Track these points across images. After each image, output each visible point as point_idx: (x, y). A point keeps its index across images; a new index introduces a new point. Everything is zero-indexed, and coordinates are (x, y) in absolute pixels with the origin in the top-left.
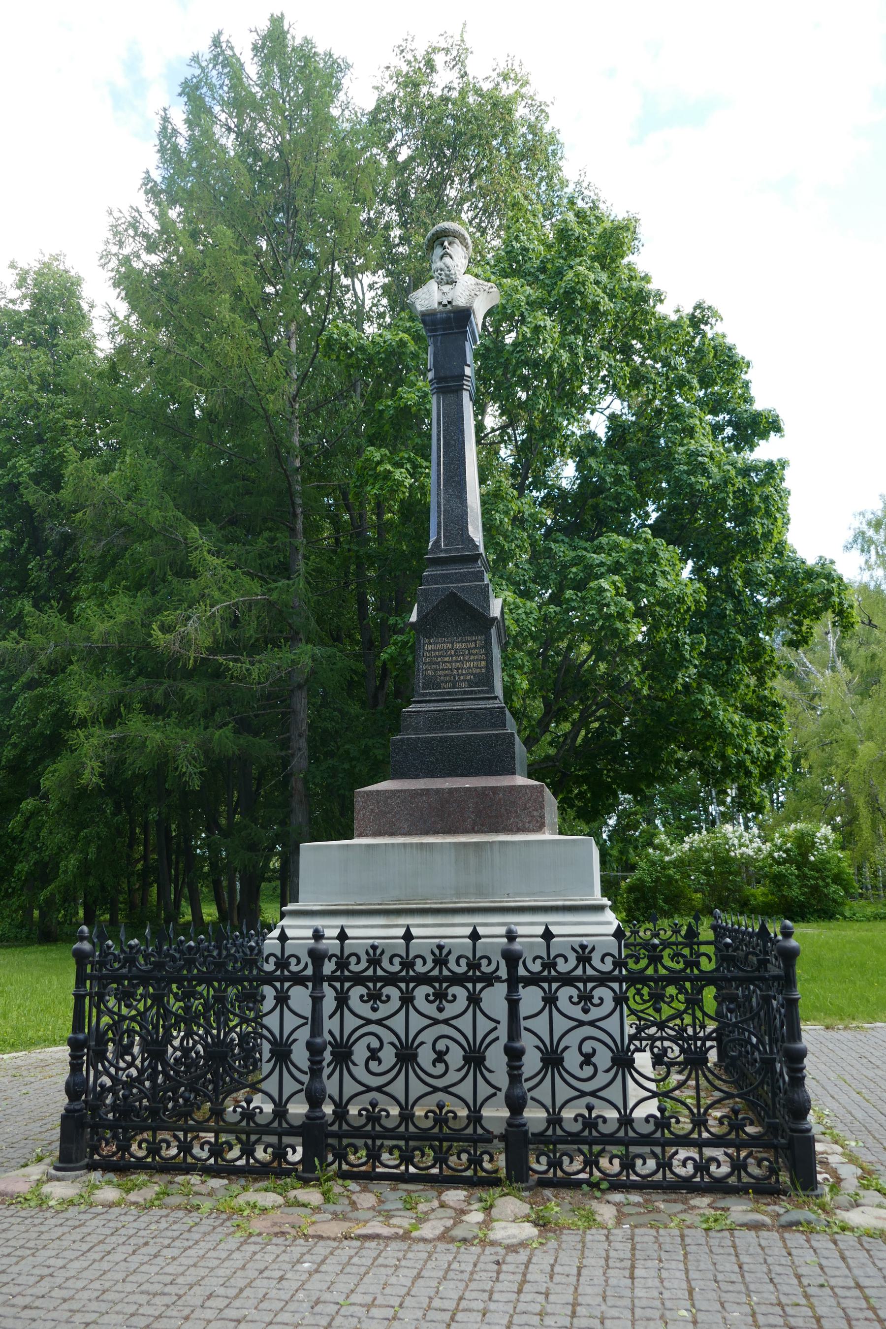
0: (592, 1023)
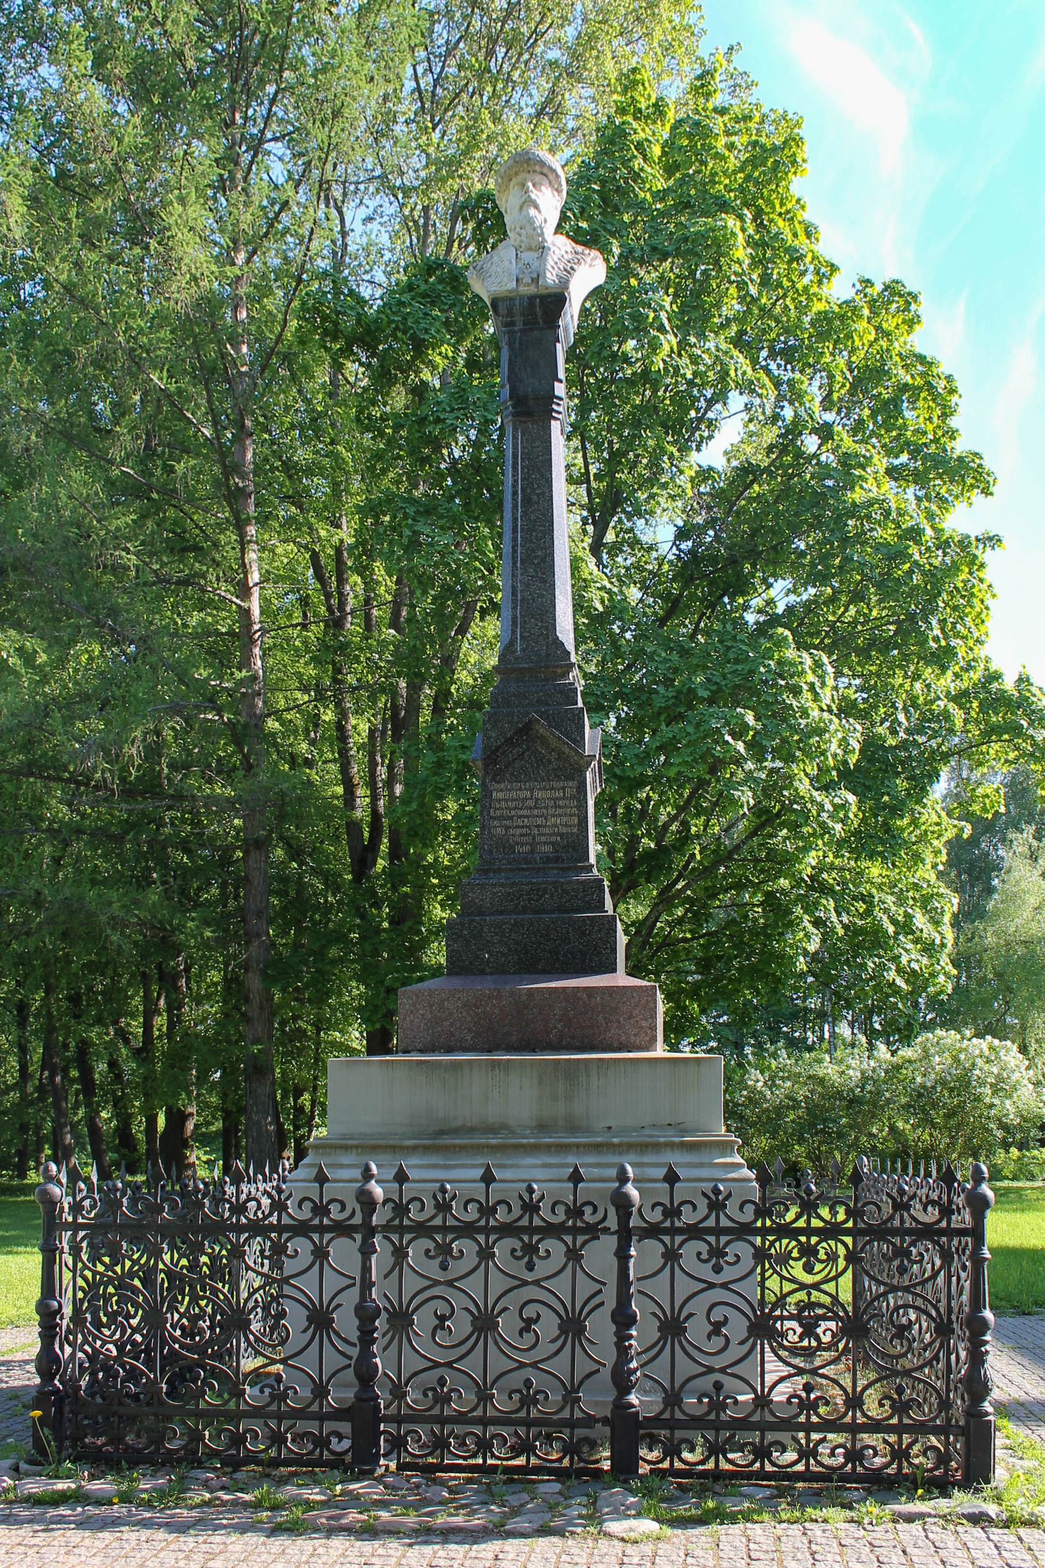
0: (725, 1286)
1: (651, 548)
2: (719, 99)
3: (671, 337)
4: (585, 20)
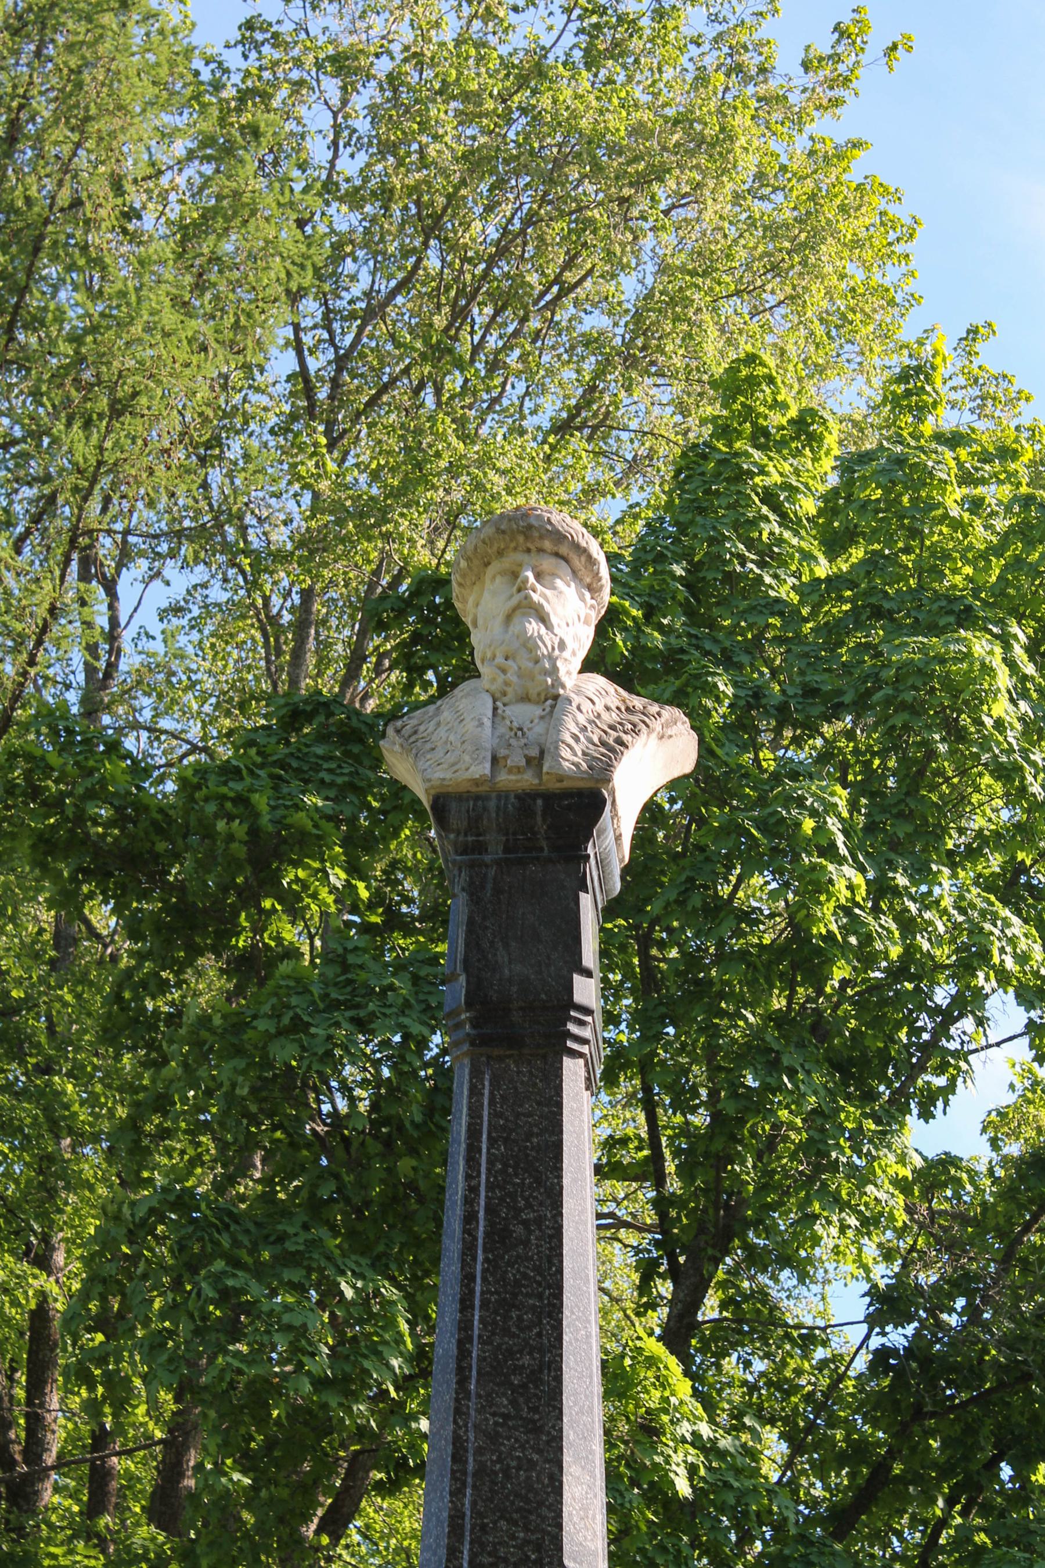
1: (809, 1339)
2: (945, 419)
3: (848, 871)
4: (664, 269)
